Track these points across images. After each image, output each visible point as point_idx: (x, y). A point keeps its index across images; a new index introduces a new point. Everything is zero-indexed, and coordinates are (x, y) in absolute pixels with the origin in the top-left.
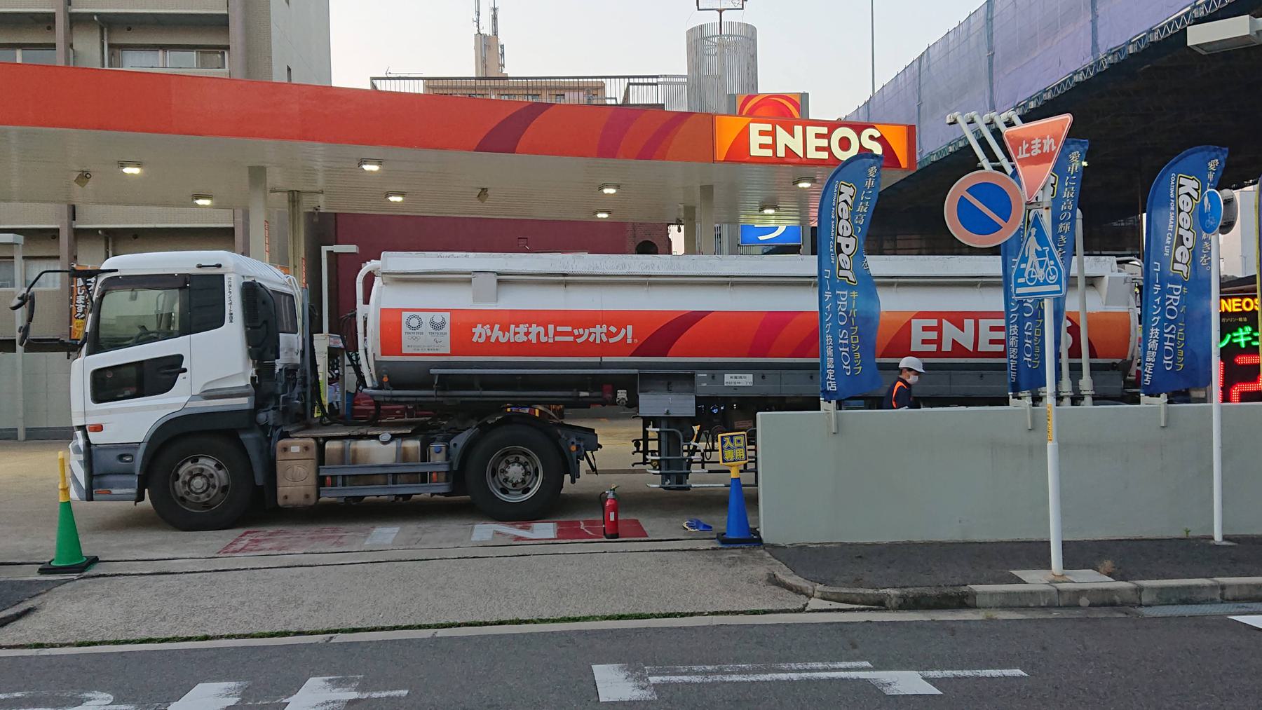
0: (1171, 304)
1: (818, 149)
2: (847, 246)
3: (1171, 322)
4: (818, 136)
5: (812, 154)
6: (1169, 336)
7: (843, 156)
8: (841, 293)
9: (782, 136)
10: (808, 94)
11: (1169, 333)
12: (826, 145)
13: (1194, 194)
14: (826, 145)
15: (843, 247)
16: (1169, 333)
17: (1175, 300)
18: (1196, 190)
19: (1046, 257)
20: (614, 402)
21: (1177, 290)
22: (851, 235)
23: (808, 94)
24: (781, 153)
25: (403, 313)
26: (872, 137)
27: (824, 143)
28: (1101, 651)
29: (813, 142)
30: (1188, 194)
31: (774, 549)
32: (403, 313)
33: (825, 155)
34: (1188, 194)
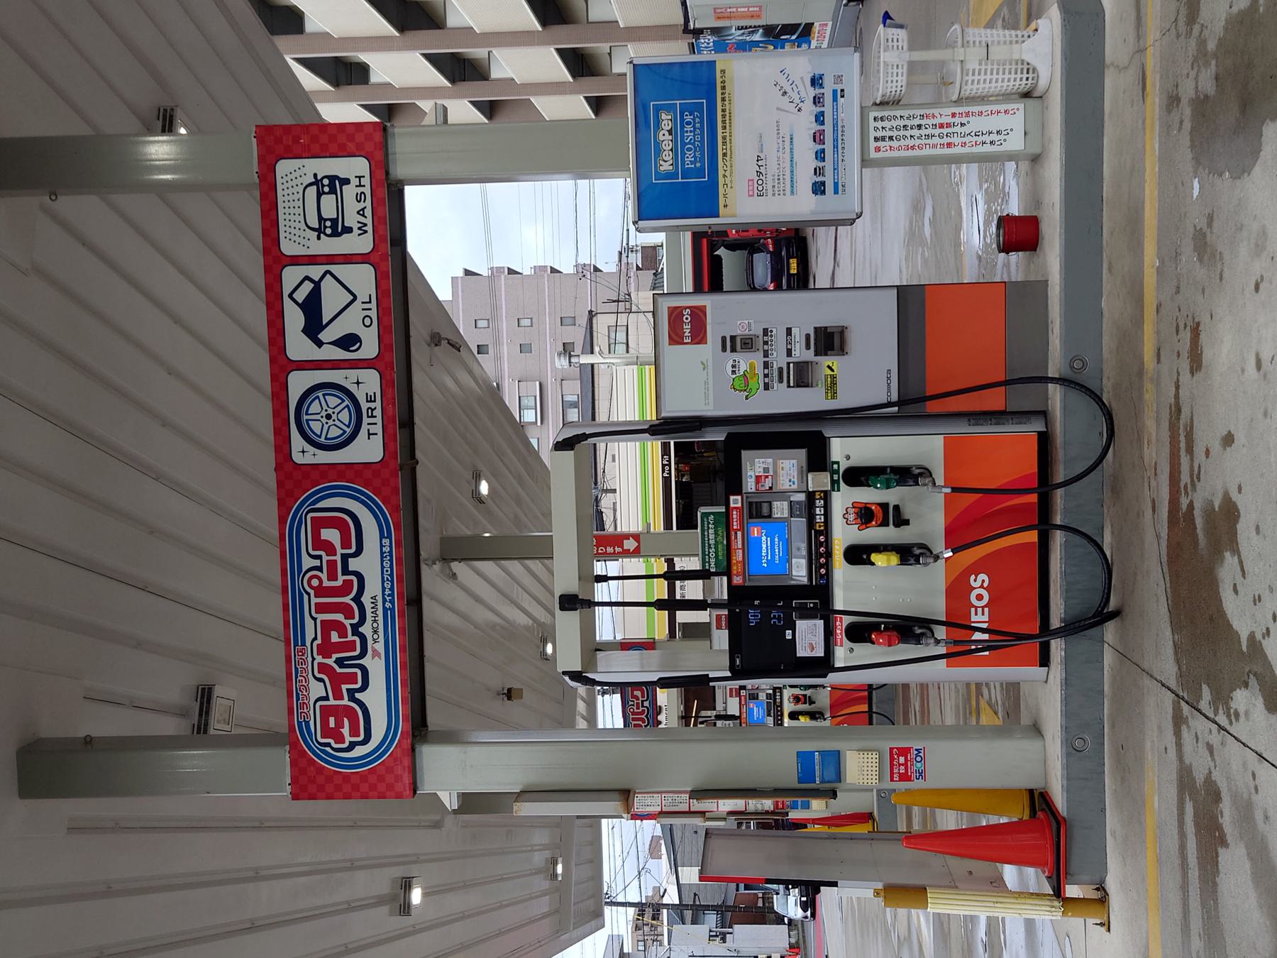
0: (690, 155)
1: (983, 614)
2: (664, 135)
3: (689, 143)
4: (976, 614)
5: (689, 327)
6: (689, 134)
7: (689, 320)
8: (690, 166)
9: (686, 334)
10: (797, 752)
11: (689, 136)
12: (319, 565)
13: (661, 162)
14: (319, 565)
15: (667, 133)
16: (689, 136)
17: (687, 157)
18: (661, 165)
19: (682, 179)
20: (802, 896)
21: (688, 164)
22: (662, 142)
23: (797, 752)
24: (690, 334)
25: (300, 302)
26: (975, 580)
27: (980, 610)
28: (1269, 798)
29: (687, 327)
30: (666, 161)
31: (326, 343)
32: (300, 302)
33: (986, 610)
34: (666, 161)
